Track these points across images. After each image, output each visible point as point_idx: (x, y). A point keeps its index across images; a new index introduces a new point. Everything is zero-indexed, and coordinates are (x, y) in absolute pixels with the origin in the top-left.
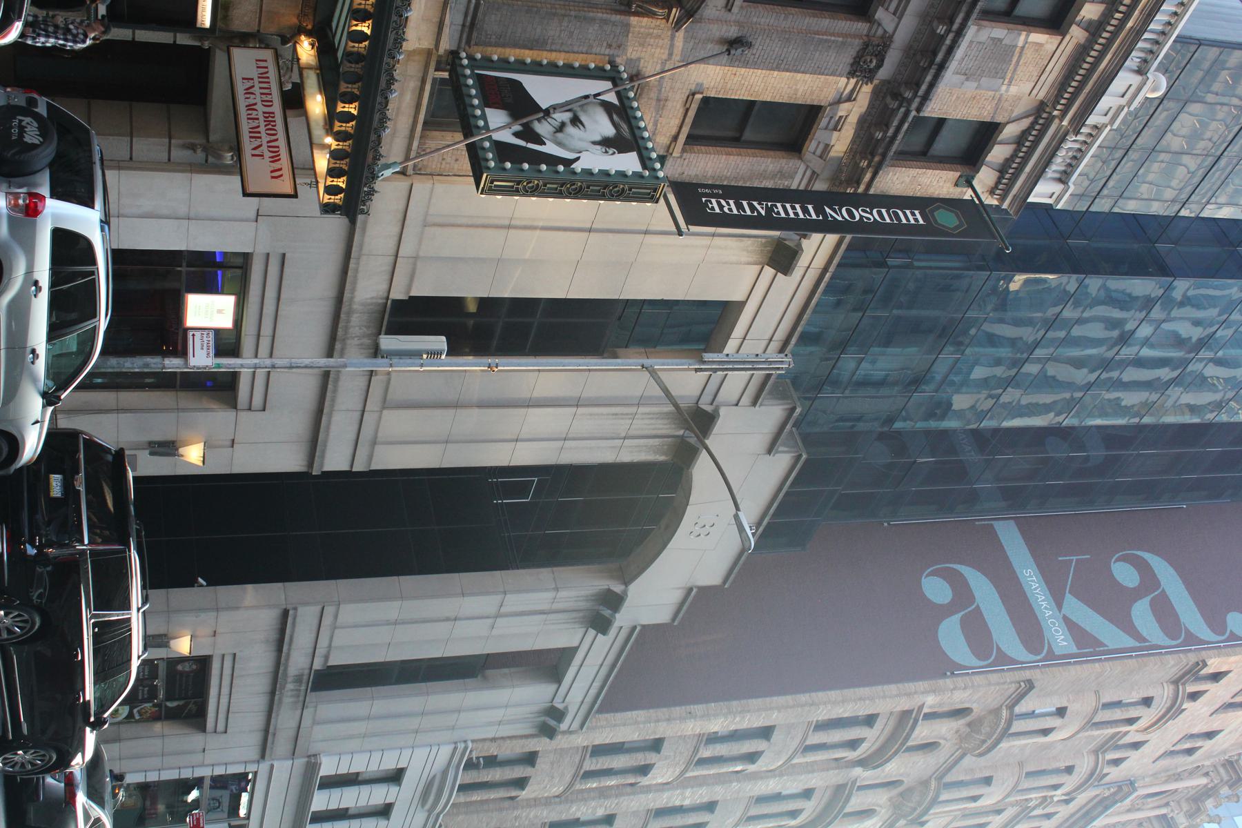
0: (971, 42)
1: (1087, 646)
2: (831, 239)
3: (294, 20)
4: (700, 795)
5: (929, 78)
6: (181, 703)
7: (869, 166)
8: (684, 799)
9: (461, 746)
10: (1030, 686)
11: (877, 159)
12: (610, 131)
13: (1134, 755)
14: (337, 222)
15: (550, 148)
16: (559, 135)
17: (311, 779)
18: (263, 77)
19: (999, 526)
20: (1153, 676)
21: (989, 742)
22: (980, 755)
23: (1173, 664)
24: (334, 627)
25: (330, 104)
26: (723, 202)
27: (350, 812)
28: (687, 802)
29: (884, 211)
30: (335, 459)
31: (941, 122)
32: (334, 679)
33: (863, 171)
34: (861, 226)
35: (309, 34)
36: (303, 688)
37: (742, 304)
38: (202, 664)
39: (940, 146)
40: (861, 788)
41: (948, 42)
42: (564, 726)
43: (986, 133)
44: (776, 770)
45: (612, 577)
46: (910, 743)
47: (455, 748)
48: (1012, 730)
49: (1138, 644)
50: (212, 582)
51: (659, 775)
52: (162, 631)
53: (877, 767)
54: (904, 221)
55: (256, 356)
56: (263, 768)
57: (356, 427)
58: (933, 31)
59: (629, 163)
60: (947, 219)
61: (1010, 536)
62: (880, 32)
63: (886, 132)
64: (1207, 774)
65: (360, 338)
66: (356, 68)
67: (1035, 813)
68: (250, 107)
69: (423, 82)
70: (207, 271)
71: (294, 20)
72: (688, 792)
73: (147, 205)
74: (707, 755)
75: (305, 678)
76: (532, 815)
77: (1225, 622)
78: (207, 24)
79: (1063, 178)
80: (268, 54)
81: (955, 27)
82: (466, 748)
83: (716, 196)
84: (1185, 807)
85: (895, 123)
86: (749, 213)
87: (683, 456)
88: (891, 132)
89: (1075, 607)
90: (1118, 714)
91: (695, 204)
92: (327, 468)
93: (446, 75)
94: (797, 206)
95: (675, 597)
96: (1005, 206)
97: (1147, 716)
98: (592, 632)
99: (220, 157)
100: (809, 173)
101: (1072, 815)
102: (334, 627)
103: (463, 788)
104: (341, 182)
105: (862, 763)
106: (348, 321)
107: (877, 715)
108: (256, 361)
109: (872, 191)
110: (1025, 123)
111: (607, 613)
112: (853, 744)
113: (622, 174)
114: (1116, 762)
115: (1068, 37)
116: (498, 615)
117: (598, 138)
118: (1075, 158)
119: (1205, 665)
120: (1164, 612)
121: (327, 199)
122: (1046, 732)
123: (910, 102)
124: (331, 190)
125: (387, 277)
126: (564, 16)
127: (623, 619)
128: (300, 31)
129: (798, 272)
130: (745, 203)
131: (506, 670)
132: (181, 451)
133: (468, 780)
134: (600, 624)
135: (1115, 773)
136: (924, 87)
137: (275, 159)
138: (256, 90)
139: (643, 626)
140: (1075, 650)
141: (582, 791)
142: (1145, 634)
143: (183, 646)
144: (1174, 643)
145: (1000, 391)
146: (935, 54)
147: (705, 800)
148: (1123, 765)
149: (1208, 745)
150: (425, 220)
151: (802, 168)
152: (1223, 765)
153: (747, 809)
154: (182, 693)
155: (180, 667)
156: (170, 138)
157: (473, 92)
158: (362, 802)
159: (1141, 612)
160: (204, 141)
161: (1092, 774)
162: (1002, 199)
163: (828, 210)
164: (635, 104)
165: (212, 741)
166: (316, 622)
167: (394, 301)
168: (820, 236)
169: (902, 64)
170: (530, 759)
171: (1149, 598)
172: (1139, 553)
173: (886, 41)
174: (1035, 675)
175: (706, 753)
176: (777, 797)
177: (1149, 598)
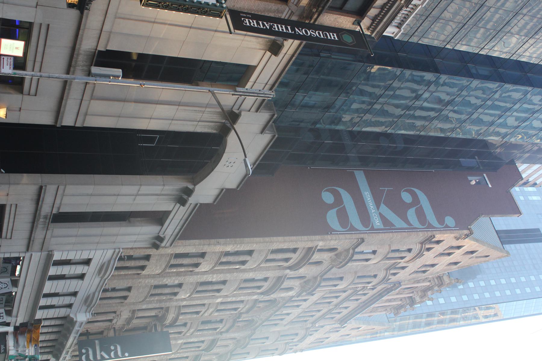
1: (388, 225)
2: (297, 42)
7: (316, 11)
8: (213, 278)
10: (363, 240)
11: (320, 9)
13: (402, 272)
14: (75, 13)
17: (49, 261)
20: (413, 241)
22: (339, 268)
23: (422, 236)
24: (63, 195)
26: (251, 21)
28: (214, 280)
29: (321, 32)
30: (68, 120)
32: (62, 218)
34: (310, 38)
36: (48, 221)
37: (255, 67)
42: (163, 244)
51: (203, 268)
53: (295, 270)
54: (329, 38)
55: (33, 71)
56: (28, 255)
60: (348, 39)
61: (361, 177)
64: (430, 281)
65: (82, 66)
72: (215, 276)
75: (49, 217)
76: (146, 282)
79: (399, 26)
84: (420, 294)
87: (224, 131)
89: (384, 209)
92: (64, 124)
94: (283, 26)
95: (216, 192)
96: (373, 36)
97: (409, 256)
100: (290, 12)
102: (63, 195)
103: (117, 268)
105: (290, 268)
106: (77, 58)
107: (298, 248)
109: (316, 23)
111: (185, 197)
112: (287, 260)
114: (395, 274)
116: (137, 195)
118: (405, 18)
119: (434, 237)
127: (192, 200)
129: (281, 55)
130: (260, 22)
131: (139, 219)
134: (182, 201)
135: (393, 279)
139: (201, 204)
140: (382, 227)
142: (411, 222)
144: (423, 227)
147: (222, 279)
149: (432, 269)
151: (287, 9)
152: (437, 278)
153: (240, 284)
158: (72, 272)
159: (411, 214)
162: (372, 32)
163: (296, 29)
166: (55, 192)
170: (147, 258)
171: (415, 208)
172: (413, 189)
176: (253, 280)
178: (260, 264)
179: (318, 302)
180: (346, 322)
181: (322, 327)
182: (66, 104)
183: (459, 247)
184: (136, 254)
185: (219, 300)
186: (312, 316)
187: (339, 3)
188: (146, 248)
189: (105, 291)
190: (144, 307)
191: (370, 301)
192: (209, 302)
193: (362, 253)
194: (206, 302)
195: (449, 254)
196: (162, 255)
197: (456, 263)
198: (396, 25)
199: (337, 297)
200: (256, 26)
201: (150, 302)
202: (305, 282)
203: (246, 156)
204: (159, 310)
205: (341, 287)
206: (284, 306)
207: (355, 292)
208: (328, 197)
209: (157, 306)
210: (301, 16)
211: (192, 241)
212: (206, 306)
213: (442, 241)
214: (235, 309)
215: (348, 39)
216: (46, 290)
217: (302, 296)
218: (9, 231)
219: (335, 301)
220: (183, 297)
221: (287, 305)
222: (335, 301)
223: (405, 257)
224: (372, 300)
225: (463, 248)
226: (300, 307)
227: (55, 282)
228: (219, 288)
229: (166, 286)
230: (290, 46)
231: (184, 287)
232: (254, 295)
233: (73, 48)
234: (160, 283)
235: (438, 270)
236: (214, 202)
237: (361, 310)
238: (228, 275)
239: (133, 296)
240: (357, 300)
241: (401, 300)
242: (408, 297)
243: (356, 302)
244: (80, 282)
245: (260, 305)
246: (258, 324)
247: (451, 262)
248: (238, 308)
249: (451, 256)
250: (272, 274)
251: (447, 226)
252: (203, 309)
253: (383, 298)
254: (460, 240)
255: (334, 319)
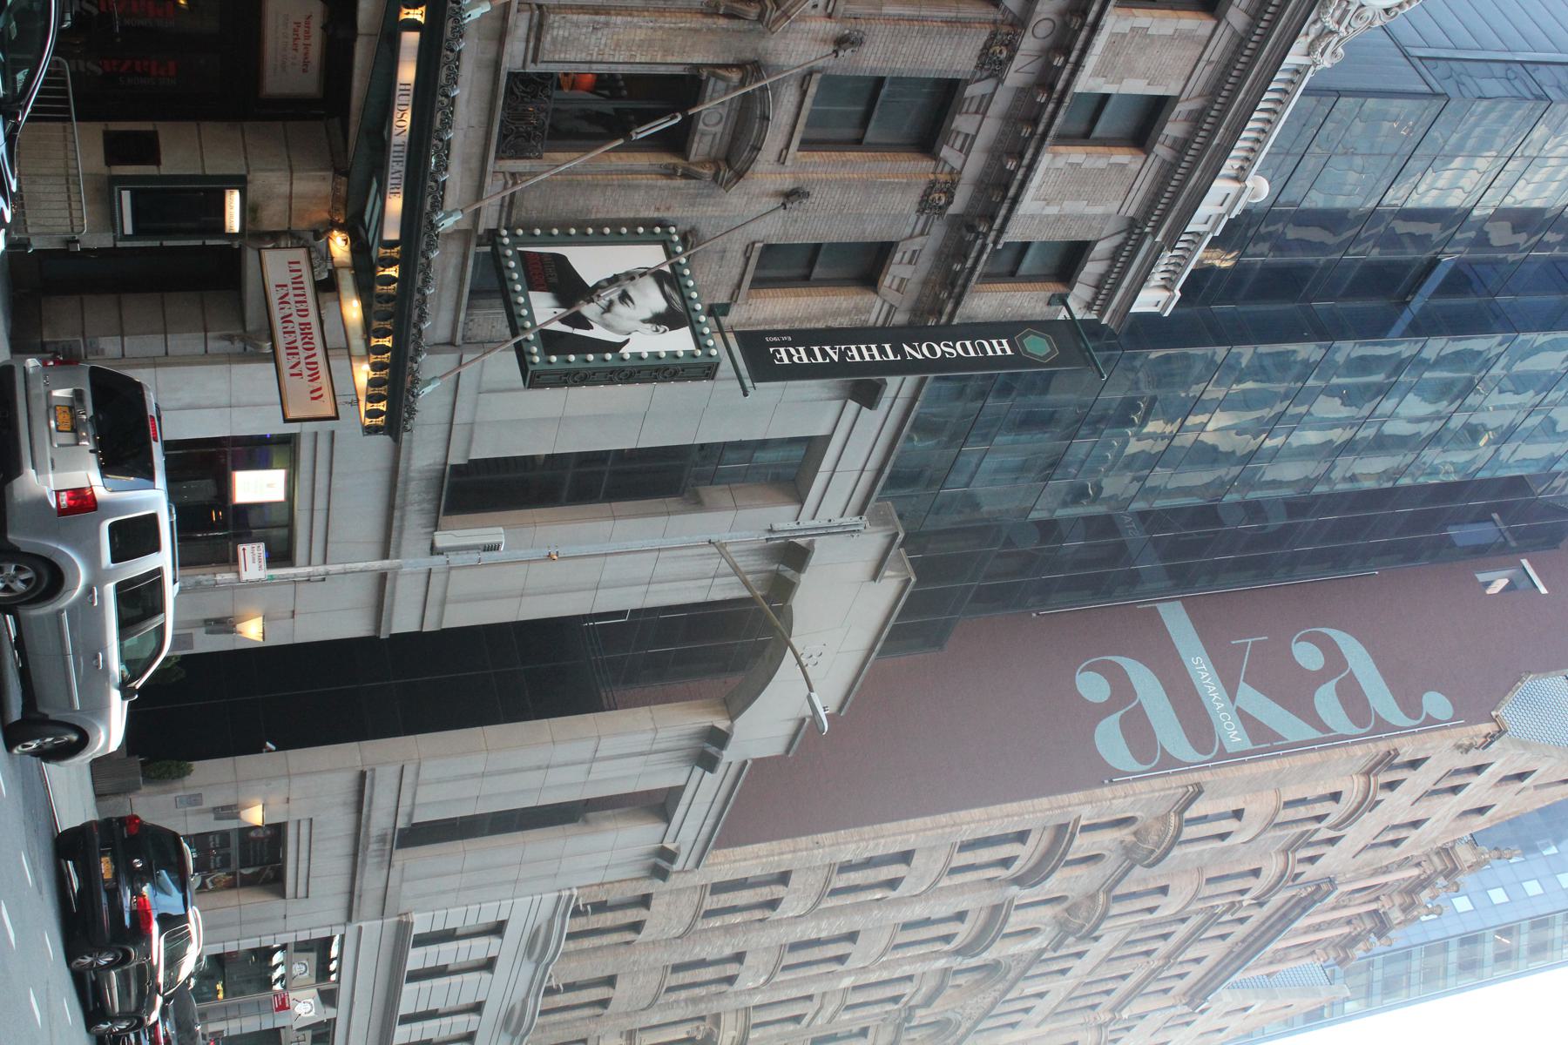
0: (1048, 169)
1: (1263, 739)
2: (911, 380)
3: (326, 216)
4: (841, 926)
5: (1003, 212)
6: (257, 869)
7: (949, 297)
8: (820, 930)
9: (566, 893)
10: (1199, 791)
11: (957, 290)
12: (660, 305)
13: (1330, 851)
14: (383, 440)
15: (598, 333)
16: (607, 316)
17: (403, 939)
18: (297, 281)
19: (1163, 609)
20: (1342, 772)
21: (1158, 852)
22: (1150, 866)
23: (1364, 753)
24: (416, 785)
25: (366, 308)
26: (792, 351)
27: (459, 932)
28: (823, 935)
30: (404, 620)
31: (1025, 246)
32: (417, 835)
33: (944, 302)
34: (945, 364)
35: (341, 228)
36: (388, 847)
37: (826, 440)
38: (276, 833)
39: (1027, 266)
40: (1019, 907)
41: (1019, 176)
42: (677, 866)
43: (1155, 109)
44: (927, 893)
45: (717, 713)
46: (1069, 857)
47: (559, 898)
48: (1112, 913)
49: (1321, 735)
50: (282, 746)
51: (787, 910)
52: (231, 801)
53: (1032, 886)
54: (990, 353)
55: (309, 564)
56: (351, 931)
57: (423, 589)
58: (1003, 167)
59: (679, 341)
60: (1037, 346)
61: (1175, 618)
62: (947, 169)
63: (964, 263)
64: (1418, 864)
65: (420, 503)
66: (389, 307)
67: (1225, 918)
68: (286, 319)
69: (465, 257)
70: (255, 451)
71: (326, 216)
72: (824, 924)
73: (186, 397)
74: (841, 883)
75: (389, 838)
76: (652, 958)
77: (1420, 705)
78: (236, 229)
80: (300, 254)
81: (1026, 162)
82: (571, 896)
83: (785, 344)
84: (1398, 900)
85: (973, 255)
86: (820, 360)
87: (781, 589)
88: (969, 263)
89: (1249, 697)
90: (1302, 812)
91: (760, 356)
92: (395, 631)
93: (488, 249)
94: (873, 347)
95: (788, 728)
96: (1104, 321)
97: (1336, 811)
98: (852, 406)
99: (260, 347)
101: (1268, 918)
102: (416, 785)
103: (572, 936)
104: (382, 406)
105: (1018, 881)
106: (406, 490)
107: (1029, 831)
108: (309, 569)
109: (956, 321)
110: (1118, 240)
111: (713, 750)
112: (1006, 863)
113: (674, 355)
114: (1312, 860)
115: (1152, 157)
116: (594, 760)
117: (648, 315)
118: (1242, 168)
119: (1397, 755)
120: (1352, 698)
121: (368, 422)
122: (1223, 836)
123: (986, 236)
124: (370, 414)
125: (443, 444)
126: (606, 186)
127: (731, 755)
128: (333, 225)
129: (884, 404)
130: (816, 349)
131: (609, 812)
132: (239, 627)
133: (576, 929)
134: (708, 762)
135: (1310, 872)
136: (998, 221)
137: (314, 377)
138: (291, 298)
139: (756, 762)
140: (1249, 746)
141: (706, 930)
142: (1329, 723)
143: (255, 816)
144: (1363, 731)
145: (1146, 472)
146: (1007, 189)
147: (845, 930)
148: (1319, 863)
149: (1414, 834)
150: (479, 386)
151: (878, 303)
152: (1438, 853)
153: (893, 936)
154: (259, 861)
155: (253, 834)
156: (206, 331)
157: (516, 276)
158: (462, 958)
159: (1326, 700)
160: (239, 331)
161: (1282, 876)
162: (1101, 313)
163: (907, 348)
164: (687, 272)
165: (291, 905)
166: (396, 781)
167: (453, 467)
168: (898, 379)
169: (974, 199)
170: (645, 901)
171: (1335, 681)
172: (1324, 630)
173: (956, 174)
174: (1204, 777)
175: (840, 881)
176: (927, 922)
177: (1335, 681)
178: (935, 882)
179: (1116, 954)
180: (1205, 999)
181: (1142, 1017)
182: (394, 587)
183: (1478, 769)
184: (614, 896)
185: (847, 982)
186: (1108, 992)
187: (1079, 126)
188: (637, 879)
189: (550, 991)
190: (656, 1019)
191: (1257, 939)
192: (821, 990)
193: (1204, 819)
194: (811, 990)
195: (1455, 790)
196: (679, 891)
197: (1481, 811)
198: (1233, 173)
199: (1165, 937)
200: (806, 360)
201: (669, 1006)
202: (1067, 910)
203: (811, 689)
204: (696, 1024)
205: (1167, 913)
206: (1023, 976)
207: (1212, 918)
208: (1092, 687)
209: (690, 1012)
210: (915, 311)
211: (749, 848)
212: (817, 1001)
213: (1424, 760)
214: (895, 1000)
215: (1037, 346)
216: (405, 1008)
217: (1068, 946)
218: (302, 881)
219: (1163, 947)
220: (751, 985)
221: (1030, 973)
222: (1163, 947)
223: (1327, 815)
224: (1264, 933)
225: (1490, 769)
226: (1070, 974)
227: (425, 984)
228: (797, 1012)
229: (702, 963)
230: (897, 388)
231: (748, 960)
232: (937, 959)
233: (394, 471)
234: (687, 959)
235: (1434, 835)
236: (788, 751)
237: (1238, 963)
238: (857, 918)
239: (621, 994)
240: (1223, 937)
241: (1349, 922)
242: (1369, 913)
243: (1220, 943)
244: (486, 976)
245: (958, 982)
246: (962, 1030)
247: (1466, 808)
248: (902, 996)
249: (1462, 795)
250: (976, 902)
251: (1430, 720)
252: (808, 1009)
253: (1295, 925)
254: (1473, 751)
255: (1171, 993)
